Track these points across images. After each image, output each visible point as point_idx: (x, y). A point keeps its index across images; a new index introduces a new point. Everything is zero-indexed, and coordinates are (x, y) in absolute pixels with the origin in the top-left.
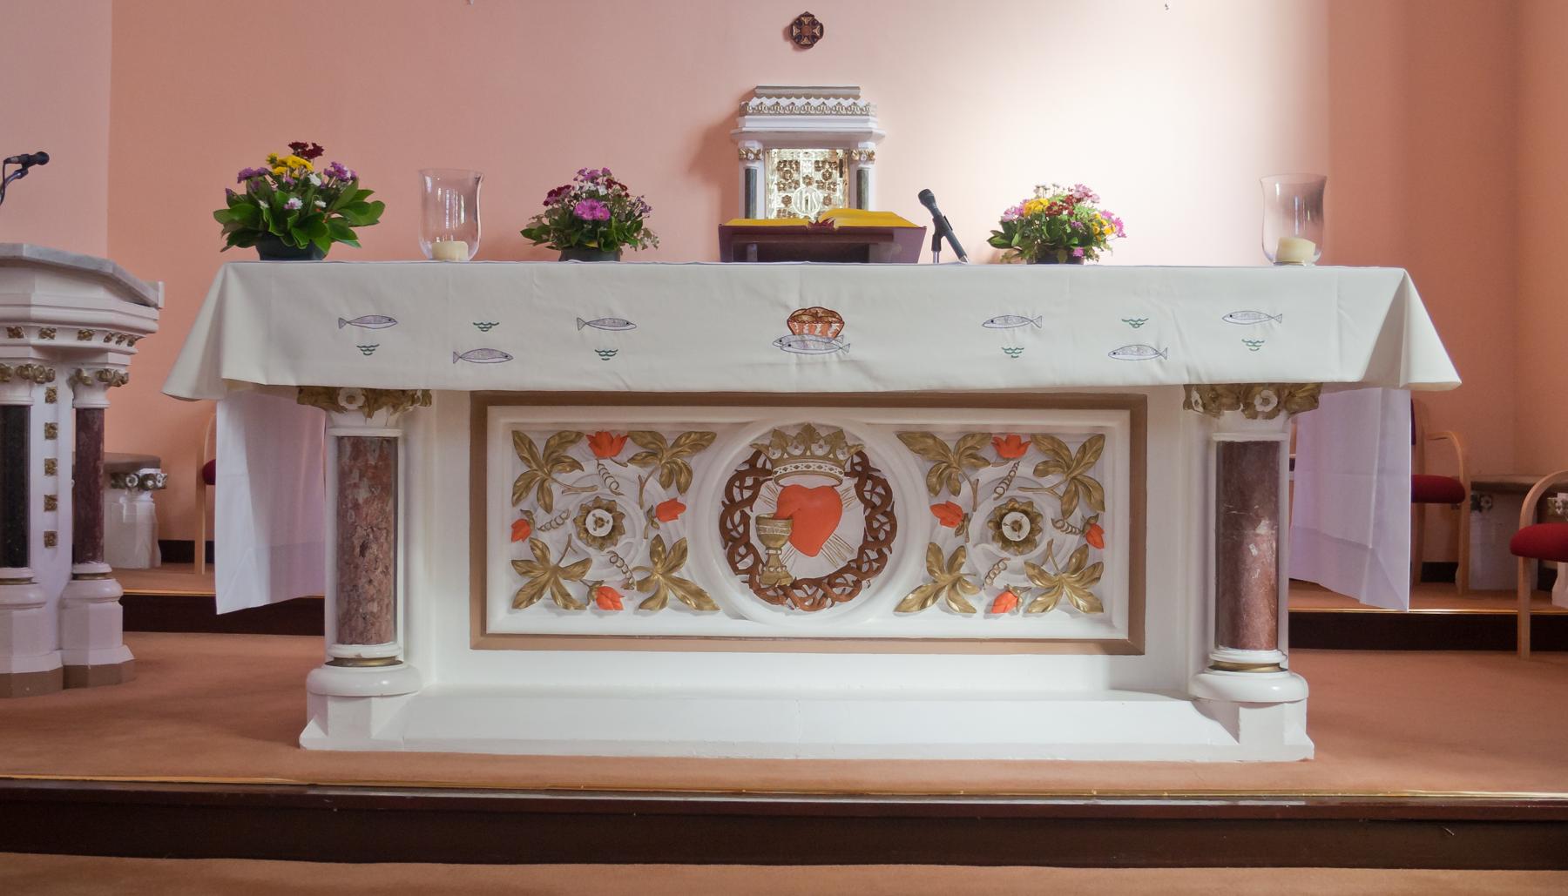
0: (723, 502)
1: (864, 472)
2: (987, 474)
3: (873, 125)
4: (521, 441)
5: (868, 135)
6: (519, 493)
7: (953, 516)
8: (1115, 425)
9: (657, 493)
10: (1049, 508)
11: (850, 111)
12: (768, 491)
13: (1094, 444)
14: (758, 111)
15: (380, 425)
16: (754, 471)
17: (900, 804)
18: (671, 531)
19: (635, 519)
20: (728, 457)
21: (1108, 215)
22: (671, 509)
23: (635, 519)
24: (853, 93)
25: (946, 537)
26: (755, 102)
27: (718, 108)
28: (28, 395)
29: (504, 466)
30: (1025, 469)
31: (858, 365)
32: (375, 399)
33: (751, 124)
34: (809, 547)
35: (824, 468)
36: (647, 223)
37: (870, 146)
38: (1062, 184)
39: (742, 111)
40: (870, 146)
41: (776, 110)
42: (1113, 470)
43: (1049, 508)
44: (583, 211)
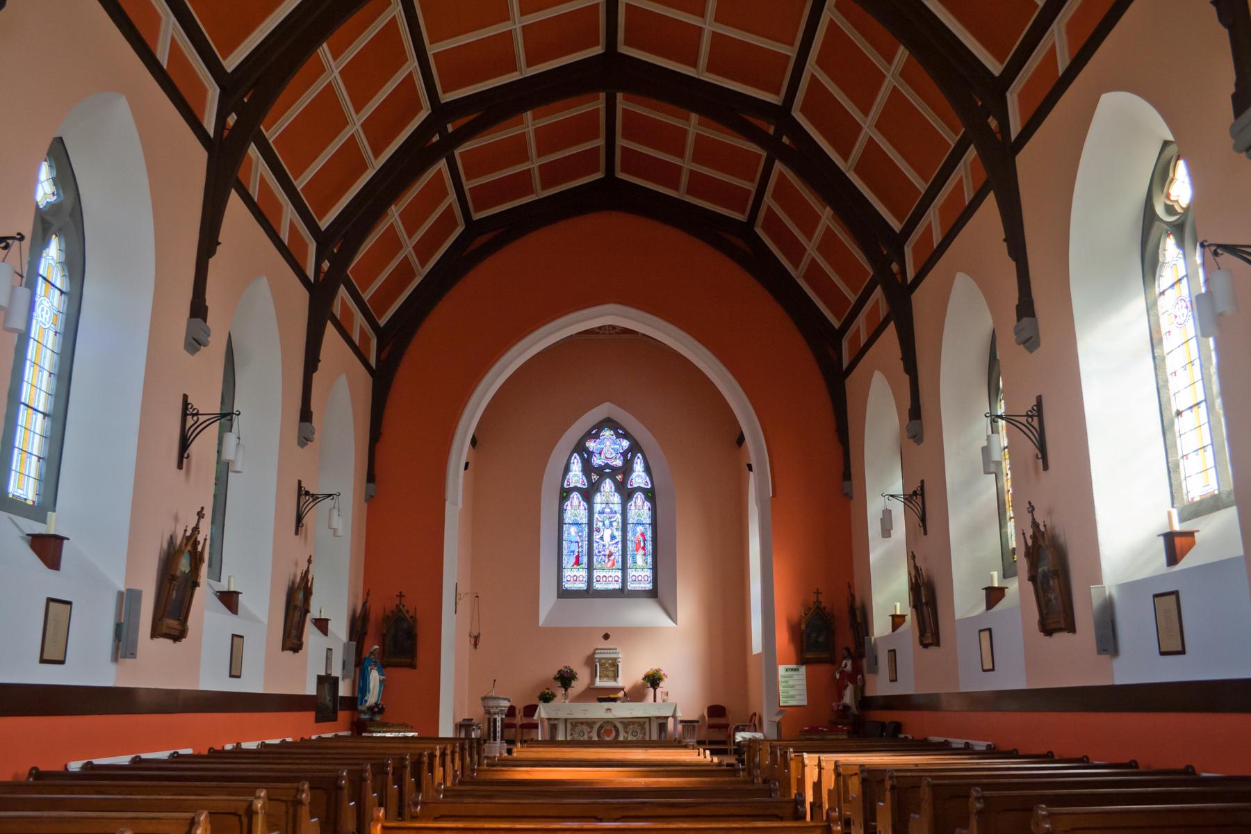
0: (295, 576)
1: (615, 727)
2: (631, 727)
3: (620, 656)
4: (571, 723)
5: (618, 658)
6: (571, 730)
7: (627, 732)
8: (647, 720)
9: (589, 730)
10: (639, 731)
11: (616, 653)
12: (603, 729)
13: (644, 723)
14: (598, 653)
15: (556, 722)
16: (601, 727)
17: (278, 159)
18: (591, 734)
19: (586, 734)
20: (598, 725)
21: (664, 674)
22: (590, 732)
23: (586, 734)
24: (616, 649)
25: (626, 735)
26: (597, 651)
27: (589, 652)
28: (496, 716)
29: (569, 726)
30: (636, 726)
31: (614, 715)
32: (556, 719)
33: (596, 656)
34: (608, 736)
35: (889, 543)
36: (577, 676)
37: (619, 660)
38: (656, 667)
39: (594, 653)
40: (619, 660)
41: (601, 653)
42: (647, 726)
43: (639, 731)
44: (565, 675)
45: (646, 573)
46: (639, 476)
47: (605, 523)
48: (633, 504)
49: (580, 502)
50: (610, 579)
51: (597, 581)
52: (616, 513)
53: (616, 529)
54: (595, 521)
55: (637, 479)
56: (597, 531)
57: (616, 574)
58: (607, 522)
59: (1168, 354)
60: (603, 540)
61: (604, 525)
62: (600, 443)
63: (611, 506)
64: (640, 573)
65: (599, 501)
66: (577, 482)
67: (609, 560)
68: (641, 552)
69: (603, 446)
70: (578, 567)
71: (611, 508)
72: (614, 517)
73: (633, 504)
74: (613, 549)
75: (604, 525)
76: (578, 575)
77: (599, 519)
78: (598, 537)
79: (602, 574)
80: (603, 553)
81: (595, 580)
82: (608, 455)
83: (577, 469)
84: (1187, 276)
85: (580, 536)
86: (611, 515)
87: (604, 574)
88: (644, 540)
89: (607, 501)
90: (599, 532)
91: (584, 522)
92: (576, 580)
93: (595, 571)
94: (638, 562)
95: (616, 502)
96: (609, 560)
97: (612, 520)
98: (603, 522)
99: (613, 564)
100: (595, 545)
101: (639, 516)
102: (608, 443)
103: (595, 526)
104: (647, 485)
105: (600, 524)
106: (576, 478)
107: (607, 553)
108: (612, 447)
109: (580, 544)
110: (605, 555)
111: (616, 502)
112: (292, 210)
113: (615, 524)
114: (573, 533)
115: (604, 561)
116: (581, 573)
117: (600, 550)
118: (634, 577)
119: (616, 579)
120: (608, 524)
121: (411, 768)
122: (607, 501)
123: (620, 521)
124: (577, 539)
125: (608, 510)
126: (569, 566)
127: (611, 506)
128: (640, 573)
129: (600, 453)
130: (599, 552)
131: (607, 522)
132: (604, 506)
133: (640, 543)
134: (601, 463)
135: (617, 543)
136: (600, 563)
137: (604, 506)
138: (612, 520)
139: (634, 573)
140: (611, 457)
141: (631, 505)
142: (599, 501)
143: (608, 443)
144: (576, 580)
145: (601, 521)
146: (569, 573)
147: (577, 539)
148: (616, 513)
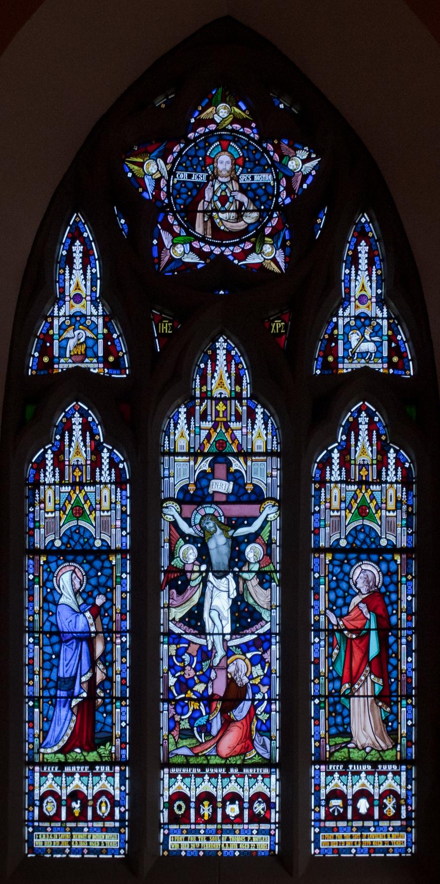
45: (390, 783)
46: (363, 321)
47: (212, 545)
48: (336, 455)
49: (97, 451)
50: (233, 810)
51: (174, 819)
52: (257, 497)
53: (260, 574)
54: (165, 536)
55: (354, 338)
56: (172, 584)
57: (259, 787)
58: (219, 544)
59: (75, 627)
60: (202, 632)
61: (204, 555)
62: (189, 162)
63: (237, 465)
64: (363, 782)
65: (182, 444)
66: (88, 350)
67: (227, 724)
68: (370, 684)
69: (199, 177)
70: (92, 756)
71: (235, 477)
72: (251, 520)
73: (336, 455)
74: (240, 667)
75: (204, 555)
76: (90, 794)
77: (184, 526)
78: (178, 613)
79: (193, 787)
80: (200, 688)
81: (164, 817)
82: (226, 220)
83: (85, 291)
84: (374, 514)
85: (96, 612)
86: (236, 510)
87: (206, 786)
88: (385, 629)
89: (221, 443)
90: (181, 591)
91: (115, 544)
92: (83, 817)
93: (165, 773)
94: (355, 728)
95: (259, 444)
96: (227, 724)
97: (242, 531)
98: (201, 543)
99: (247, 743)
100: (166, 650)
101: (363, 511)
102: (224, 162)
103: (165, 562)
104: (402, 366)
105: (189, 553)
106: (83, 334)
107: (219, 687)
108: (244, 179)
109: (99, 648)
110: (207, 699)
111: (259, 444)
112: (393, 787)
113: (253, 552)
114: (67, 598)
115: (205, 729)
116: (103, 784)
117: (189, 673)
118: (336, 802)
119: (259, 808)
120: (225, 550)
121: (339, 418)
122: (221, 443)
123: (276, 536)
124: (85, 622)
125: (221, 486)
126: (50, 753)
127: (237, 465)
128: (363, 782)
129: (189, 214)
130: (184, 685)
131: (219, 544)
132: (204, 465)
133: (364, 638)
134: (191, 258)
135: (263, 642)
136: (186, 734)
137: (204, 465)
138: (242, 531)
139: (336, 783)
140: (241, 225)
141: (328, 461)
142: (182, 444)
143: (224, 162)
144: (83, 817)
145: (191, 540)
146: (49, 783)
147: (85, 622)
148: (257, 497)
